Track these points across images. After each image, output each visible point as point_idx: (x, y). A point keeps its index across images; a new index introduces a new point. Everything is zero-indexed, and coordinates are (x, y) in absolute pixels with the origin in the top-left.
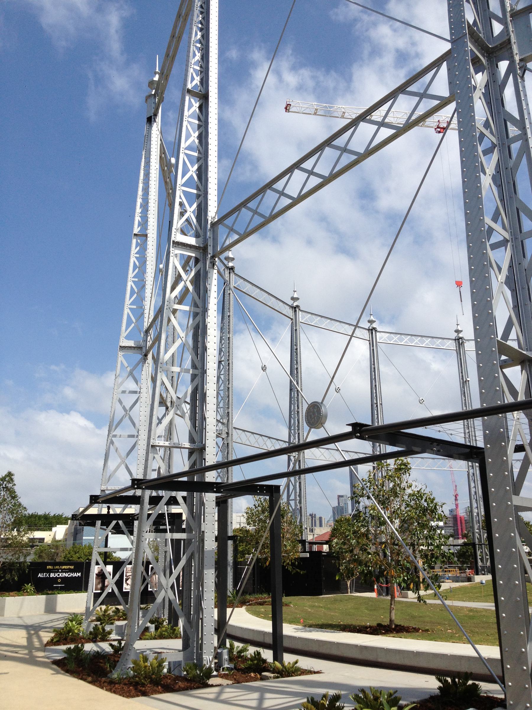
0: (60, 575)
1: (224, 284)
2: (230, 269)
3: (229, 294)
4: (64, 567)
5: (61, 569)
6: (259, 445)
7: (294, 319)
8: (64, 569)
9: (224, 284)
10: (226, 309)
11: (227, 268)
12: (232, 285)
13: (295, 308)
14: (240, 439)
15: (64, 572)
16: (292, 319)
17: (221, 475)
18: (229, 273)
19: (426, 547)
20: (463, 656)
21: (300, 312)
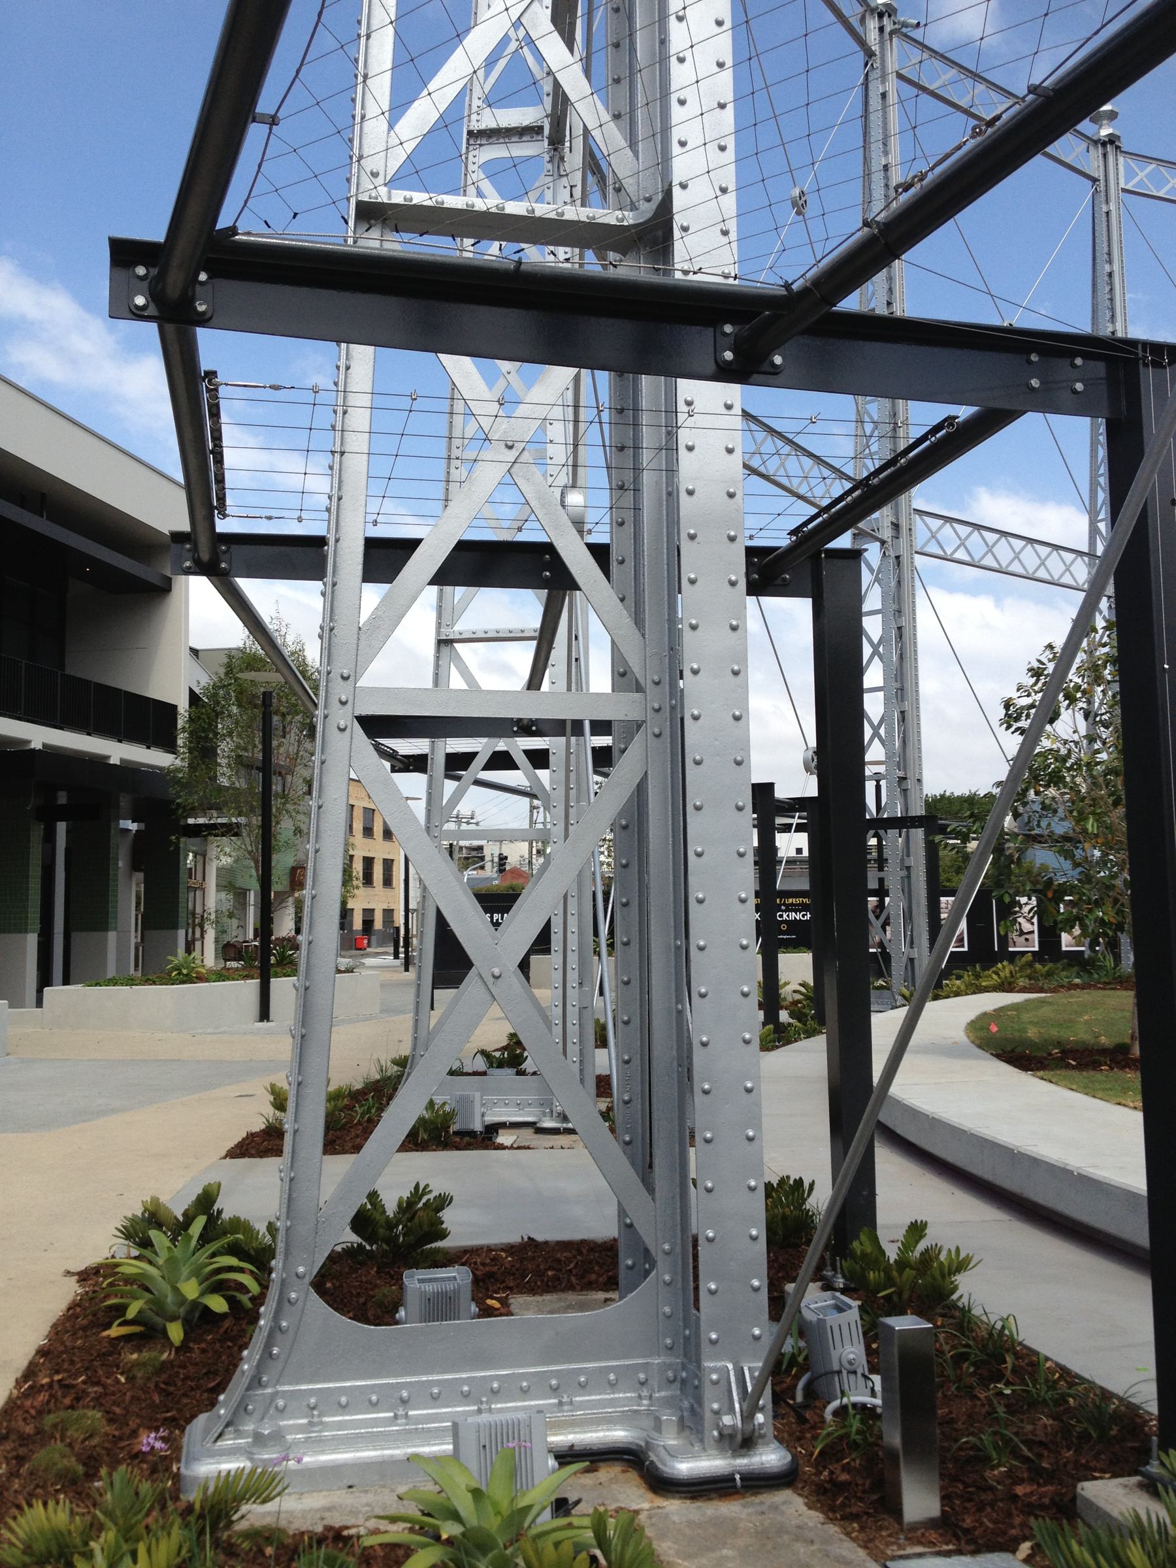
0: (785, 916)
1: (866, 65)
2: (1104, 144)
3: (1107, 213)
4: (790, 901)
5: (784, 904)
6: (942, 547)
7: (1102, 178)
8: (792, 904)
9: (866, 65)
10: (1102, 256)
11: (1096, 142)
12: (892, 64)
13: (1104, 144)
14: (939, 543)
15: (792, 911)
16: (1094, 180)
17: (881, 649)
18: (1105, 155)
19: (368, 914)
20: (986, 1140)
21: (1121, 159)
